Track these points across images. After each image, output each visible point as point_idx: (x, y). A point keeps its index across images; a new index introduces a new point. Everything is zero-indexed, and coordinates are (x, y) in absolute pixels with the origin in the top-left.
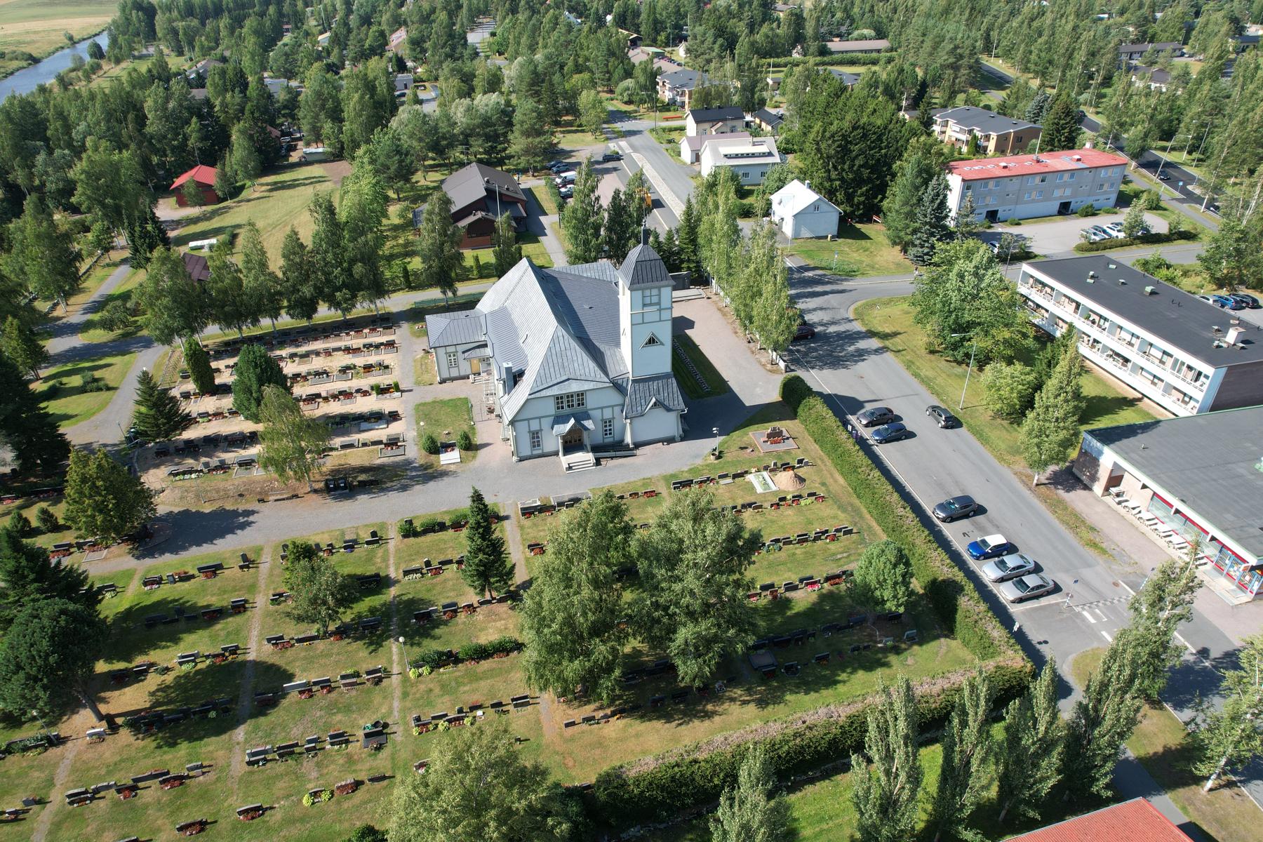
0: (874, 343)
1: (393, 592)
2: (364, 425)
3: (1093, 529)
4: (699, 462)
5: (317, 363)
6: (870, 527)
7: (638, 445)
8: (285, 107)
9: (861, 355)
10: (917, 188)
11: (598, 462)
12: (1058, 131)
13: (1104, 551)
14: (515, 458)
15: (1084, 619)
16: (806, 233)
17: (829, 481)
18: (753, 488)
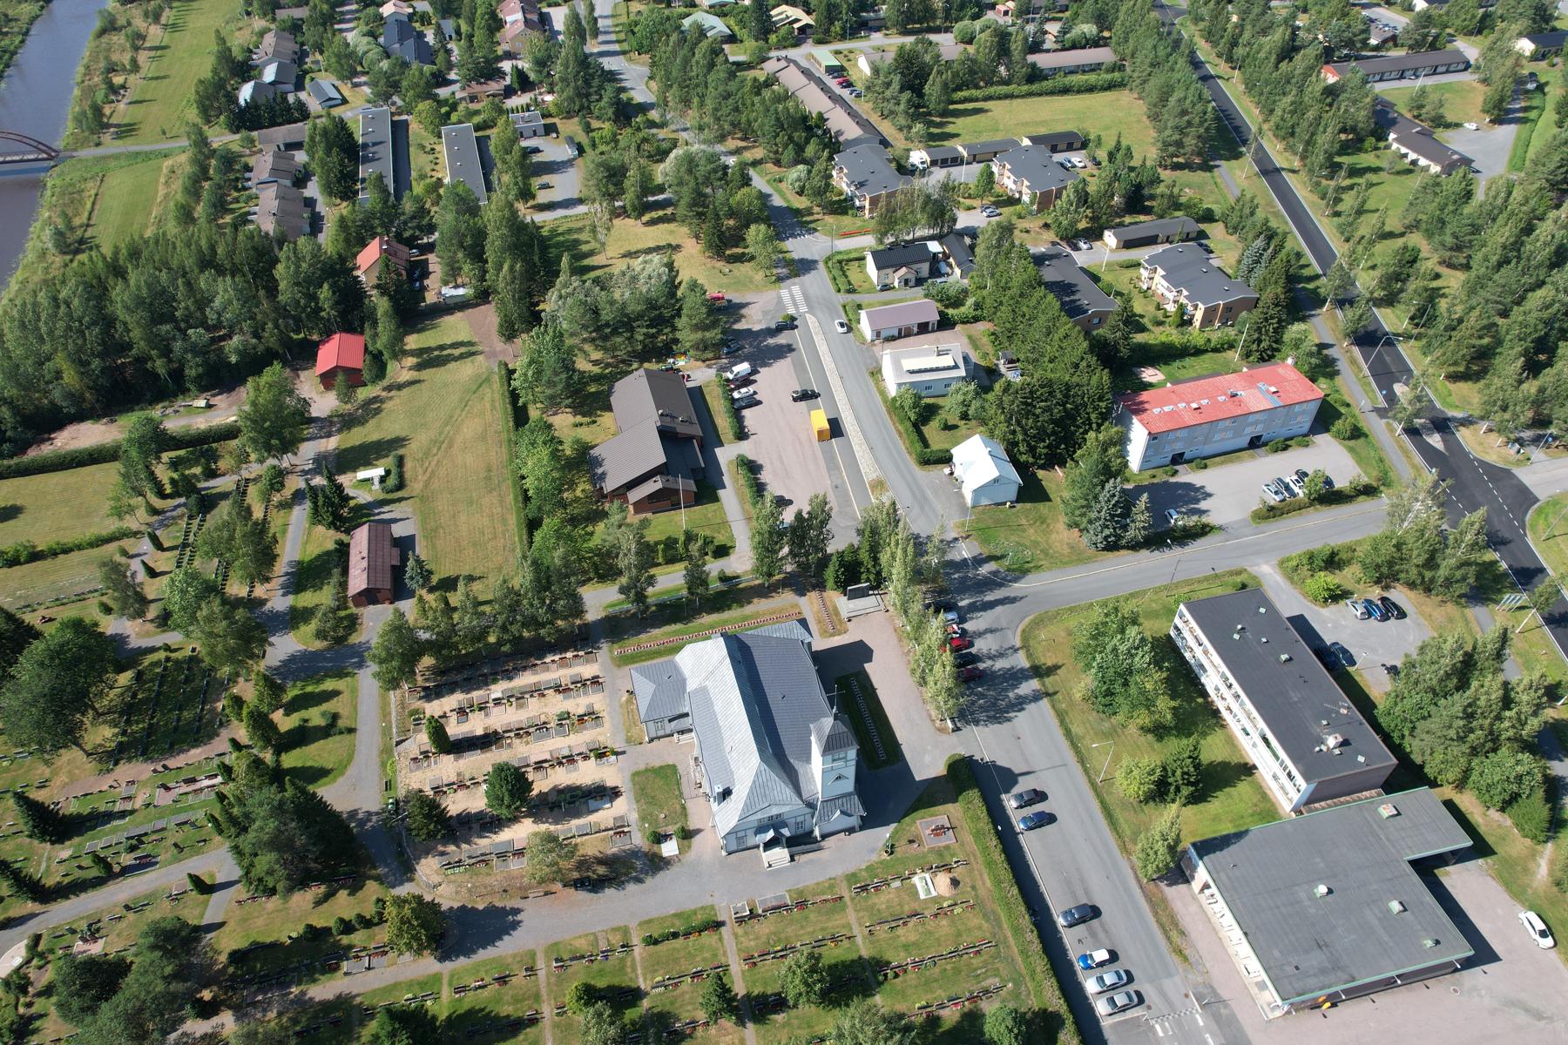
0: (1033, 685)
1: (646, 1003)
2: (592, 804)
3: (1182, 933)
4: (874, 858)
5: (535, 709)
6: (1006, 938)
7: (824, 837)
8: (413, 218)
9: (1020, 704)
10: (1095, 486)
11: (792, 859)
12: (1266, 320)
13: (1186, 959)
14: (724, 853)
15: (1155, 1033)
16: (985, 502)
17: (979, 884)
18: (917, 893)
